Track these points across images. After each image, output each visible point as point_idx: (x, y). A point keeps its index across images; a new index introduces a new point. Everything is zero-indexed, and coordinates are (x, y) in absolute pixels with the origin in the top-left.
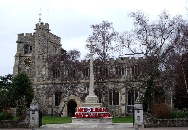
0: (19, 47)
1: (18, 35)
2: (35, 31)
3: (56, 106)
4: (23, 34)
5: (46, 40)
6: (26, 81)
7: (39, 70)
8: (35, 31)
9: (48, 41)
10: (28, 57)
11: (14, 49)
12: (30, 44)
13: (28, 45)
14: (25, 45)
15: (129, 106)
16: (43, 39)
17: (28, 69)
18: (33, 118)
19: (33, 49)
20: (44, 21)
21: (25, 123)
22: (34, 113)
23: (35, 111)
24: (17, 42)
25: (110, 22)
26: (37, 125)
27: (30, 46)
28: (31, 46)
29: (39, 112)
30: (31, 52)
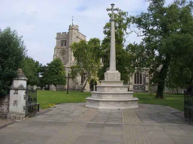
0: (57, 42)
1: (57, 33)
2: (68, 31)
3: (81, 83)
4: (60, 33)
5: (76, 37)
6: (59, 65)
7: (71, 57)
8: (68, 31)
9: (77, 38)
10: (63, 48)
11: (54, 43)
12: (65, 39)
13: (64, 41)
14: (61, 41)
15: (135, 84)
16: (74, 36)
17: (63, 57)
18: (15, 102)
19: (67, 43)
20: (75, 24)
21: (3, 110)
22: (17, 94)
23: (19, 91)
24: (56, 38)
25: (126, 12)
26: (21, 114)
27: (65, 41)
28: (66, 41)
29: (26, 93)
30: (65, 45)
